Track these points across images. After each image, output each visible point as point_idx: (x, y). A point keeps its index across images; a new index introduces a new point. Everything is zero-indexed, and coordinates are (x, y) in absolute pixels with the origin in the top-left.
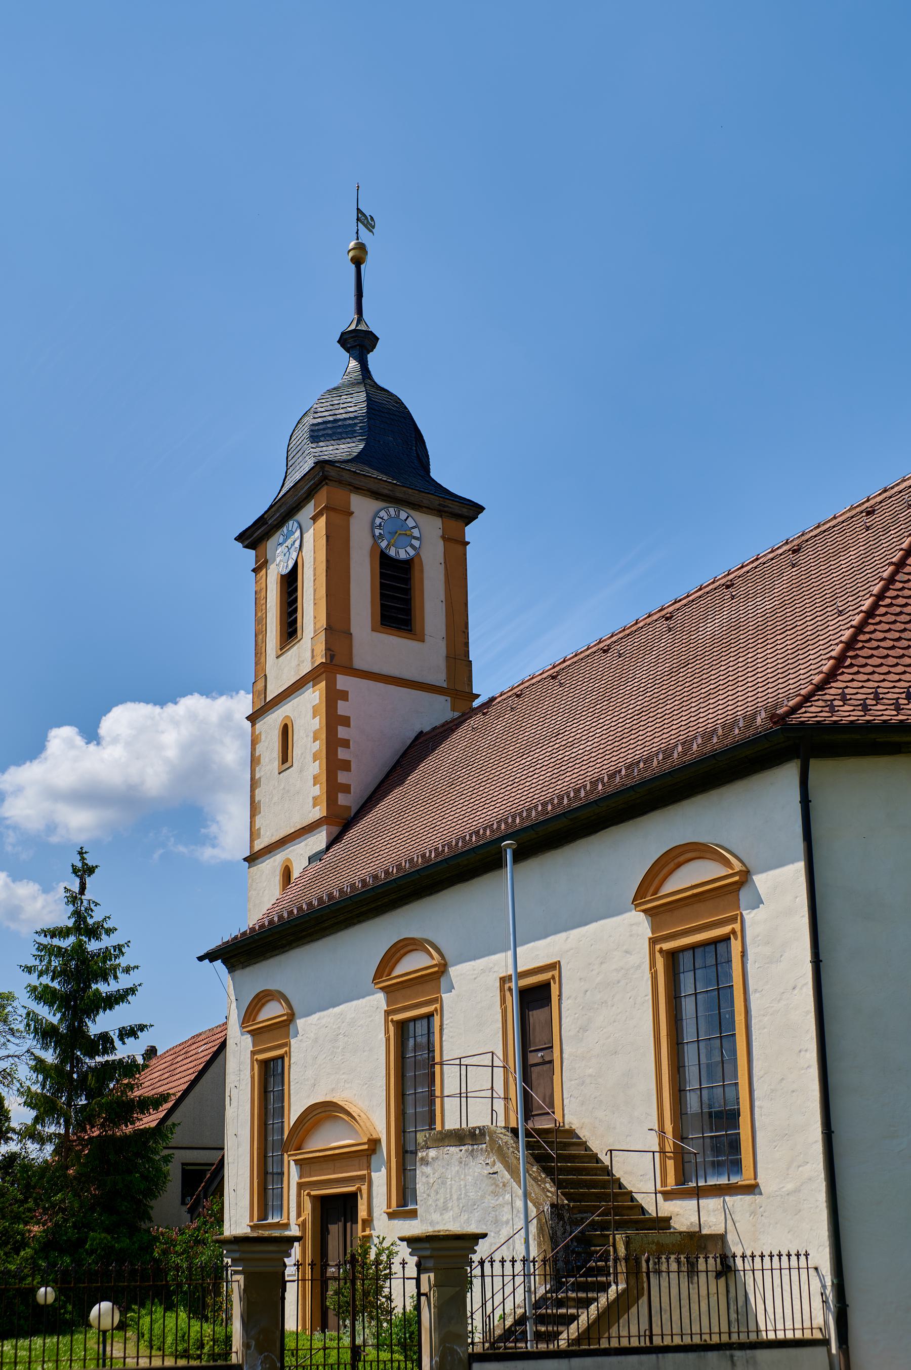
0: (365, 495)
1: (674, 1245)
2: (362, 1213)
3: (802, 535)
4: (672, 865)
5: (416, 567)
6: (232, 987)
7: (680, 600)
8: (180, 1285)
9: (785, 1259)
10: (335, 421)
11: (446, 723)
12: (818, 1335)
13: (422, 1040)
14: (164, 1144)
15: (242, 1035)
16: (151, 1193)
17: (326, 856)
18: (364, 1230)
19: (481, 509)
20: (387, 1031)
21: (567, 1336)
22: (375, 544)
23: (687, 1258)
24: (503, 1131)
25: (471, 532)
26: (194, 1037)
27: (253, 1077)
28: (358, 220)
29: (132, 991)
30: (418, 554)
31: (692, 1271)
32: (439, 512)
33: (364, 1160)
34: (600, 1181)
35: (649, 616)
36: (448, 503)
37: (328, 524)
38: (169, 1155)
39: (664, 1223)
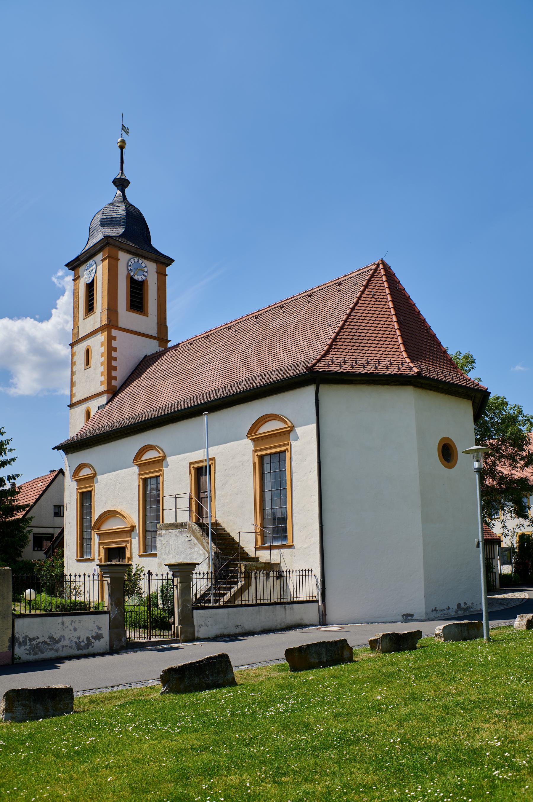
0: (124, 252)
1: (262, 567)
2: (128, 555)
3: (312, 289)
4: (263, 422)
5: (146, 284)
6: (67, 461)
7: (261, 311)
8: (45, 583)
9: (294, 572)
10: (112, 218)
11: (157, 353)
12: (314, 599)
13: (154, 486)
14: (27, 525)
15: (72, 481)
16: (23, 547)
17: (106, 407)
18: (128, 562)
19: (173, 261)
20: (139, 482)
21: (223, 601)
22: (128, 274)
23: (266, 572)
24: (194, 524)
25: (168, 270)
26: (35, 479)
27: (77, 499)
28: (122, 129)
29: (13, 460)
30: (146, 279)
31: (268, 577)
32: (155, 261)
33: (128, 534)
34: (231, 543)
35: (247, 316)
36: (159, 257)
37: (109, 264)
38: (31, 530)
39: (256, 559)
